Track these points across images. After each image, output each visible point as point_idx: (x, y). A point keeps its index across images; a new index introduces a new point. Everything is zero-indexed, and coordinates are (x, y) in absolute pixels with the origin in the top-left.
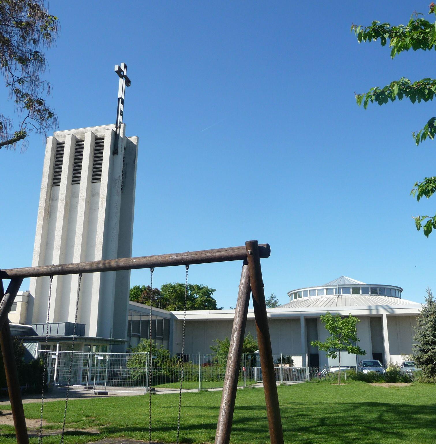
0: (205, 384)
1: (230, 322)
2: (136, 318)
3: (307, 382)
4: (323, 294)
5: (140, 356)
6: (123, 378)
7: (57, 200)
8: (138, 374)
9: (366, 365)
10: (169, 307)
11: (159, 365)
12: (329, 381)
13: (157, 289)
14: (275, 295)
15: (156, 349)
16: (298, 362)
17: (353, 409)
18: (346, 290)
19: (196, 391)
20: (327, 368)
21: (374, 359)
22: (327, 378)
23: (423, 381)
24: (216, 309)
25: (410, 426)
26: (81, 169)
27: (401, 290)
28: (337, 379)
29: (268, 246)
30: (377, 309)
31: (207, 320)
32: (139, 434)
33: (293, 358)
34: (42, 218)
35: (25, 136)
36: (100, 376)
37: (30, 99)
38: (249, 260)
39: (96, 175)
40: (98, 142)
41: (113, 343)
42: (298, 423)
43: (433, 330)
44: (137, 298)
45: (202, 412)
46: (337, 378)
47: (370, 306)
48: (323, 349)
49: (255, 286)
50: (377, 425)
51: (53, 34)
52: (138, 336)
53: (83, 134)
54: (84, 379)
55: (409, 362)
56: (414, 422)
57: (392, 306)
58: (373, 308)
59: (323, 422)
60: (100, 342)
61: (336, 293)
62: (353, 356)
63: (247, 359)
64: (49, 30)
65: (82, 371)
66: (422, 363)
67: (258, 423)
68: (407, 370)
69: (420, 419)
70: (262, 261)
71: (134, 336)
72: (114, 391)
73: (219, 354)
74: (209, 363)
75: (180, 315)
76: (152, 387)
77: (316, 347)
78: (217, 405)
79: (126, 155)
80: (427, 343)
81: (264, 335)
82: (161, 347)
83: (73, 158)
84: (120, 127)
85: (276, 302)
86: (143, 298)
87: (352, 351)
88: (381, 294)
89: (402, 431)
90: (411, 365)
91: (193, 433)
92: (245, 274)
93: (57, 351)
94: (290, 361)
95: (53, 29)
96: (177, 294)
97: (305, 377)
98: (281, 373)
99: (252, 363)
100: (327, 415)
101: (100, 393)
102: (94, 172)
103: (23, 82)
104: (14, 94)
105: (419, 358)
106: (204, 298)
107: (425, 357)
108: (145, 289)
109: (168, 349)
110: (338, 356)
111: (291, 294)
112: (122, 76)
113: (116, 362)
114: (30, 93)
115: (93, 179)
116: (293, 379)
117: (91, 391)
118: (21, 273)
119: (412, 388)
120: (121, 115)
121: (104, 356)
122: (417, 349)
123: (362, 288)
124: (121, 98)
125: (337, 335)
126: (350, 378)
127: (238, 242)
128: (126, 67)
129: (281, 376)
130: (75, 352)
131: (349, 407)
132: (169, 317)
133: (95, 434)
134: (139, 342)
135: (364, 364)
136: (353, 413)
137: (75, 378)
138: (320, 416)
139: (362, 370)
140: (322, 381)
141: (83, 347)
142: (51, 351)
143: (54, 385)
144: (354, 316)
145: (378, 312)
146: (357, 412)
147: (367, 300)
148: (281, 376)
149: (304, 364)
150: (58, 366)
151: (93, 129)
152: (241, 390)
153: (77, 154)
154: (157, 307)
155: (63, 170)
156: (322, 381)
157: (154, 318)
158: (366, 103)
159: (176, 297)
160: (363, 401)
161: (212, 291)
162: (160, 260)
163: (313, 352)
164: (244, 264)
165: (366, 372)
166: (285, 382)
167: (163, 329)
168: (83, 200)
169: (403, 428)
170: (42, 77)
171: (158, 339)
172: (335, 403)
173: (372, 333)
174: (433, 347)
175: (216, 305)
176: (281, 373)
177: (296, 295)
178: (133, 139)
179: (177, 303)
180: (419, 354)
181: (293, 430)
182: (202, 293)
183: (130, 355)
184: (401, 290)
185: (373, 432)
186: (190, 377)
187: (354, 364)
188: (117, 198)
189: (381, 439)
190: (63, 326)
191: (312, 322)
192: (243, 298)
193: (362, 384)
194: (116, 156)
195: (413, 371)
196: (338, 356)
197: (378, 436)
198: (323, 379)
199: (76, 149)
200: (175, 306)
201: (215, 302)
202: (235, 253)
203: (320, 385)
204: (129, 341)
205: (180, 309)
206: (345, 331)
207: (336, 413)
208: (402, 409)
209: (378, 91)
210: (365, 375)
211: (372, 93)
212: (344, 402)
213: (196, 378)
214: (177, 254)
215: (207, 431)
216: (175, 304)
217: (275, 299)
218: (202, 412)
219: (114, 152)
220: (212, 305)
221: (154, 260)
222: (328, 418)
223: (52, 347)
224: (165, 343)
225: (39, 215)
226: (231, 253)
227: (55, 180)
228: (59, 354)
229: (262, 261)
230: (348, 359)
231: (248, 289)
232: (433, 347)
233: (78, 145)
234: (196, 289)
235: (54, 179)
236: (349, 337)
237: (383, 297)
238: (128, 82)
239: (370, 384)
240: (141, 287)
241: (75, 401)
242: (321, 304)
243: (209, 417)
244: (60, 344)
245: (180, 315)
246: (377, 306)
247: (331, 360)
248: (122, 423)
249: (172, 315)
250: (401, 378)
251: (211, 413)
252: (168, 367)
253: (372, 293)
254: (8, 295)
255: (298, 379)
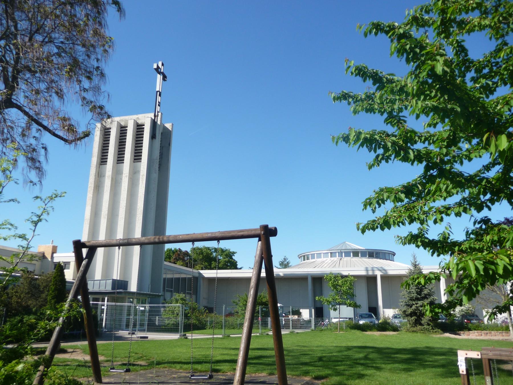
0: (228, 332)
1: (249, 280)
2: (169, 276)
3: (312, 330)
4: (328, 257)
5: (175, 307)
6: (159, 326)
7: (104, 176)
8: (172, 322)
9: (362, 317)
10: (197, 267)
11: (189, 315)
12: (331, 329)
13: (187, 251)
14: (287, 257)
15: (187, 302)
16: (306, 314)
17: (346, 351)
18: (347, 254)
19: (221, 336)
20: (329, 318)
21: (369, 312)
22: (329, 327)
23: (408, 330)
24: (236, 268)
25: (387, 362)
26: (124, 151)
27: (394, 254)
28: (337, 328)
29: (276, 229)
30: (373, 270)
31: (229, 278)
32: (178, 366)
33: (301, 311)
34: (92, 191)
35: (89, 134)
36: (140, 324)
37: (94, 106)
38: (262, 239)
39: (137, 156)
40: (139, 128)
41: (151, 297)
42: (301, 359)
43: (417, 288)
44: (170, 259)
45: (226, 352)
46: (337, 327)
47: (367, 268)
48: (326, 304)
49: (266, 256)
50: (362, 362)
51: (110, 51)
52: (171, 291)
53: (127, 121)
54: (127, 326)
55: (399, 315)
56: (390, 359)
57: (386, 268)
58: (370, 269)
59: (320, 359)
60: (140, 296)
61: (339, 256)
62: (351, 310)
63: (262, 311)
64: (107, 47)
65: (125, 320)
66: (407, 316)
67: (269, 359)
68: (397, 321)
69: (396, 357)
70: (272, 239)
71: (168, 291)
72: (152, 336)
73: (240, 306)
74: (230, 314)
75: (208, 273)
76: (185, 333)
77: (321, 302)
78: (238, 347)
79: (162, 138)
80: (412, 299)
81: (272, 293)
82: (191, 301)
83: (118, 141)
84: (158, 116)
85: (288, 263)
86: (174, 259)
87: (350, 305)
88: (377, 257)
89: (380, 365)
90: (400, 318)
91: (220, 366)
92: (259, 248)
93: (106, 303)
94: (299, 314)
95: (110, 47)
96: (203, 256)
97: (311, 327)
98: (291, 322)
99: (265, 315)
100: (324, 355)
101: (141, 337)
102: (135, 153)
103: (87, 90)
104: (80, 101)
105: (405, 312)
106: (227, 259)
107: (410, 311)
108: (176, 251)
109: (196, 302)
110: (338, 309)
111: (301, 257)
112: (160, 73)
113: (154, 312)
114: (93, 100)
115: (135, 159)
116: (300, 328)
117: (134, 336)
118: (97, 244)
119: (398, 336)
120: (159, 105)
121: (145, 307)
122: (404, 304)
123: (361, 252)
124: (159, 91)
125: (338, 292)
126: (348, 328)
127: (255, 225)
128: (163, 65)
129: (291, 325)
130: (118, 304)
131: (342, 349)
132: (197, 275)
133: (145, 366)
134: (172, 296)
135: (360, 316)
136: (346, 353)
137: (120, 325)
138: (319, 355)
139: (358, 321)
140: (325, 330)
141: (127, 300)
142: (100, 303)
143: (102, 331)
144: (352, 276)
145: (373, 272)
146: (350, 353)
147: (365, 262)
148: (291, 325)
149: (311, 315)
150: (106, 316)
151: (135, 117)
152: (257, 336)
153: (121, 138)
154: (187, 267)
155: (109, 151)
156: (325, 330)
157: (177, 276)
158: (337, 142)
159: (203, 258)
160: (355, 344)
161: (234, 253)
162: (199, 237)
163: (319, 306)
164: (259, 241)
165: (361, 322)
166: (294, 330)
167: (191, 285)
168: (126, 176)
169: (381, 364)
170: (103, 88)
171: (188, 293)
172: (331, 346)
173: (368, 289)
174: (416, 302)
175: (237, 265)
176: (291, 322)
177: (305, 257)
178: (168, 126)
179: (203, 263)
180: (405, 308)
181: (296, 364)
182: (226, 255)
183: (164, 307)
184: (394, 254)
185: (358, 366)
186: (216, 326)
187: (352, 316)
188: (155, 176)
189: (362, 370)
190: (110, 282)
191: (318, 281)
192: (257, 265)
193: (358, 333)
194: (154, 140)
195: (401, 322)
196: (338, 309)
197: (360, 369)
198: (326, 328)
199: (121, 133)
200: (202, 266)
201: (237, 262)
202: (253, 233)
203: (323, 332)
204: (164, 296)
205: (206, 268)
206: (344, 288)
207: (332, 353)
208: (385, 351)
209: (345, 136)
210: (361, 325)
211: (341, 136)
212: (341, 345)
213: (220, 326)
214: (212, 233)
215: (230, 364)
216: (202, 264)
217: (287, 261)
218: (226, 352)
219: (153, 136)
220: (233, 265)
221: (194, 237)
222: (325, 357)
223: (101, 300)
224: (194, 297)
225: (89, 189)
226: (250, 233)
227: (103, 160)
228: (107, 305)
229: (272, 239)
230: (347, 312)
231: (262, 259)
232: (416, 302)
233: (123, 131)
234: (220, 252)
235: (102, 159)
236: (347, 293)
237: (378, 260)
238: (164, 78)
239: (364, 332)
240: (173, 249)
241: (123, 343)
242: (326, 265)
243: (231, 355)
244: (108, 297)
245: (208, 273)
246: (373, 268)
247: (332, 312)
248: (164, 358)
249: (200, 273)
250: (390, 328)
251: (233, 352)
252: (196, 317)
253: (369, 256)
254: (87, 260)
255: (306, 328)
